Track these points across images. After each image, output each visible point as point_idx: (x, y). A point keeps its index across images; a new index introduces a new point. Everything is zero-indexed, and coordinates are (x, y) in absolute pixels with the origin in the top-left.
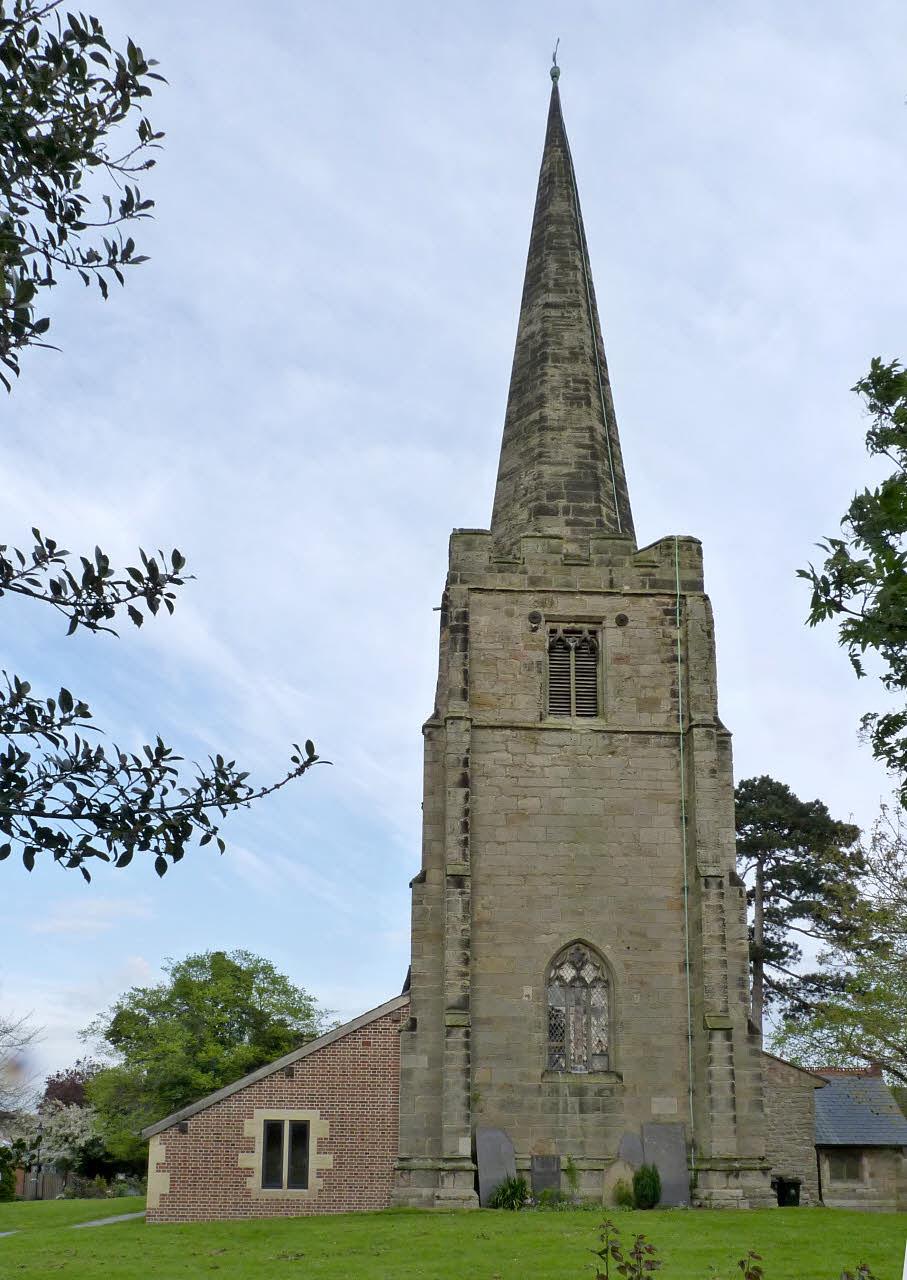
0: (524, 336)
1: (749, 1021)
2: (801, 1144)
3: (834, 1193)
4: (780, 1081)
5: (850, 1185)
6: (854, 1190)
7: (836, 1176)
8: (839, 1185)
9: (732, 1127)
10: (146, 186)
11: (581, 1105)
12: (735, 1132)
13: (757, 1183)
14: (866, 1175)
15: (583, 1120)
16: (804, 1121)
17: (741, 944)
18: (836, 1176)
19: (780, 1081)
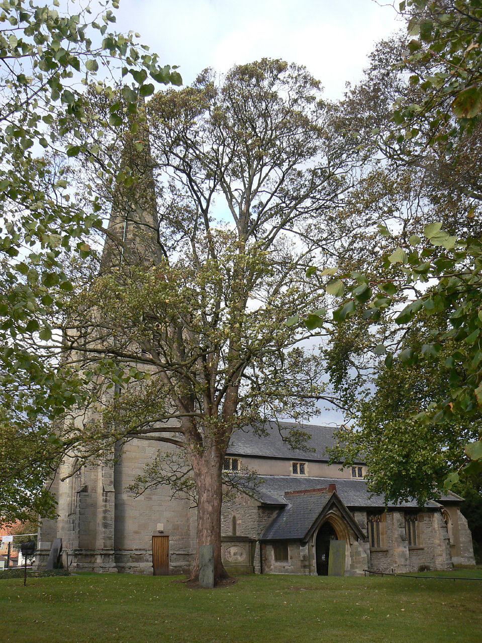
8: (278, 564)
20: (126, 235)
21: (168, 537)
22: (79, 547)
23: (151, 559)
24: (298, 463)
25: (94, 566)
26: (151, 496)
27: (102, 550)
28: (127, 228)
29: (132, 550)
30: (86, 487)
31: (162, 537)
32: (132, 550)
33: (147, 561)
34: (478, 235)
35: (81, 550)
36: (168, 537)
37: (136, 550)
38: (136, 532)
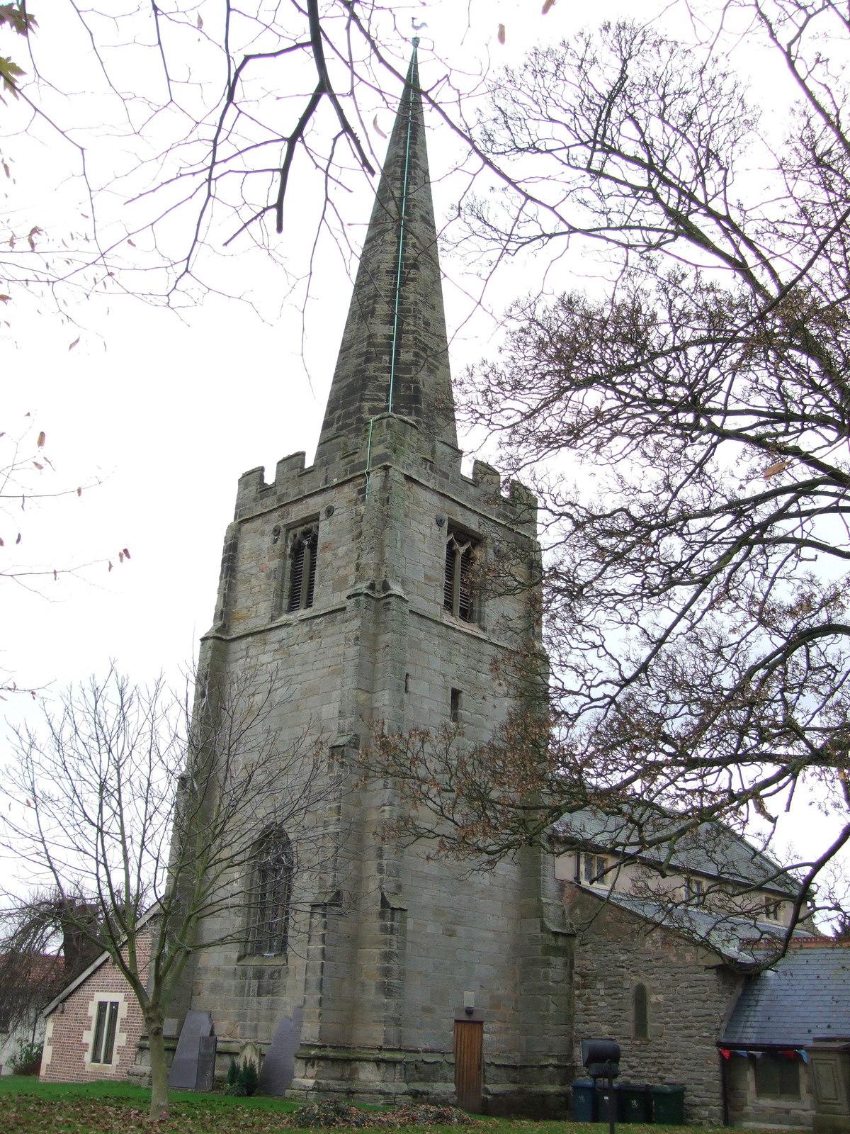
0: (425, 272)
1: (383, 895)
2: (699, 1042)
3: (761, 1115)
4: (674, 959)
5: (783, 1103)
6: (788, 1111)
7: (761, 1090)
8: (767, 1102)
9: (318, 1011)
10: (92, 296)
11: (259, 987)
12: (320, 1015)
13: (372, 1077)
14: (803, 1089)
15: (259, 1003)
16: (703, 1012)
17: (384, 811)
18: (761, 1090)
19: (674, 959)
20: (398, 354)
21: (481, 1023)
22: (320, 1039)
23: (451, 1075)
24: (720, 388)
25: (353, 1087)
26: (455, 927)
27: (380, 1049)
28: (399, 338)
29: (417, 1052)
30: (338, 894)
31: (469, 1022)
32: (417, 1052)
33: (445, 1080)
34: (846, 727)
35: (324, 1047)
36: (481, 1023)
37: (426, 1051)
38: (427, 1010)
